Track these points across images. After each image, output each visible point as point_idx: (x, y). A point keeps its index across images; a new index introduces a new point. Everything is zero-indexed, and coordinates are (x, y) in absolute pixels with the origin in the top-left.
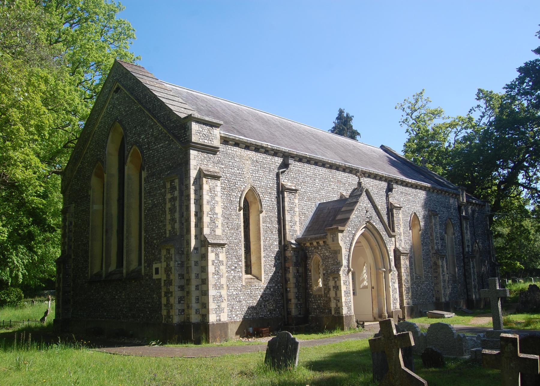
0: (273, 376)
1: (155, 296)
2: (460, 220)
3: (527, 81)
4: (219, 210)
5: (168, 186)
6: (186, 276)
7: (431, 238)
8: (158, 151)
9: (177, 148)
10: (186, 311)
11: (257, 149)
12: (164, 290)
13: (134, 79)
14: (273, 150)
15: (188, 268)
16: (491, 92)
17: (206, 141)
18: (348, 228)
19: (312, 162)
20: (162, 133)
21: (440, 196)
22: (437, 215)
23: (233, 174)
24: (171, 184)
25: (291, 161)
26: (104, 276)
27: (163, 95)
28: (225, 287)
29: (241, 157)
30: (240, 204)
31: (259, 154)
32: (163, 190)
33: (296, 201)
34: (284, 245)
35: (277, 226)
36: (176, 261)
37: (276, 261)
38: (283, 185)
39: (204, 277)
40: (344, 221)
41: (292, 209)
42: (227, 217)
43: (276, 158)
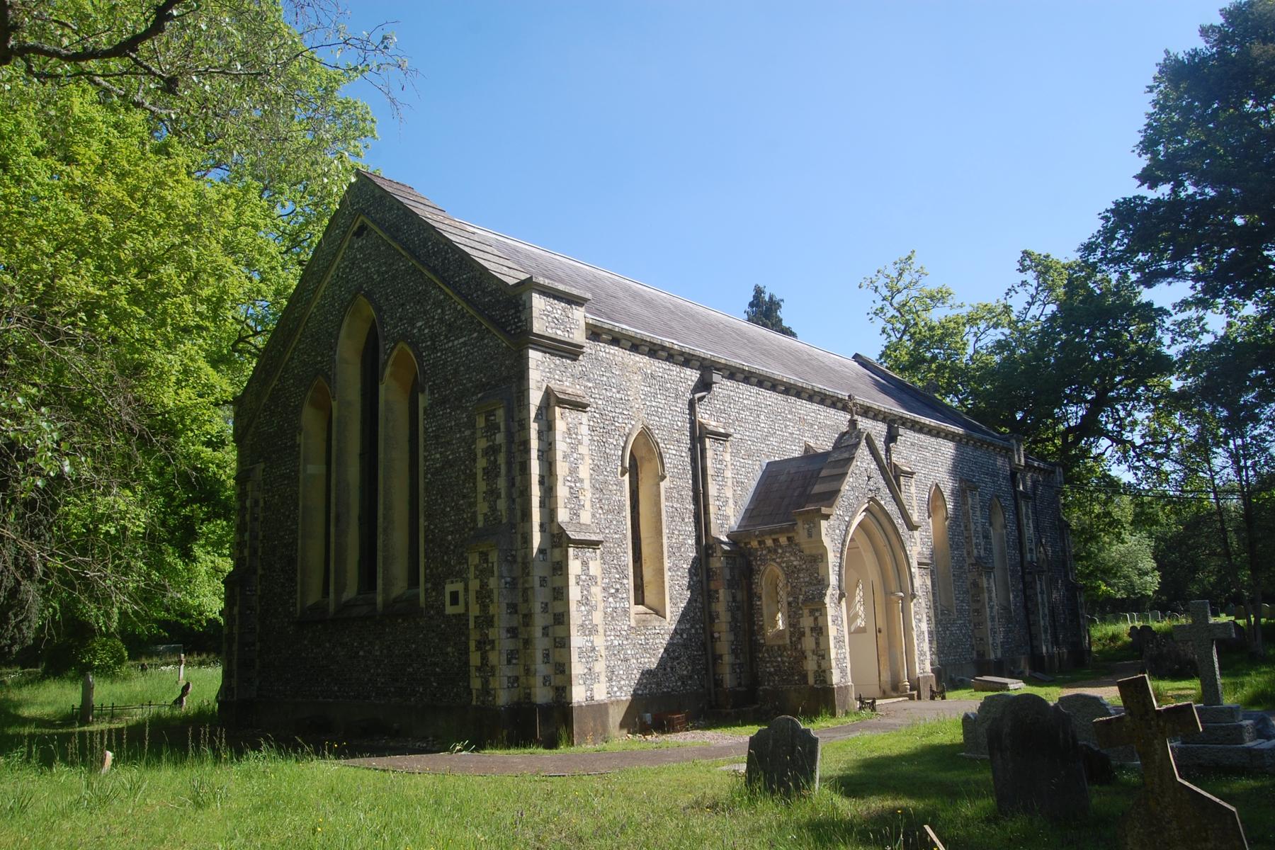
0: (769, 811)
1: (449, 649)
2: (1015, 499)
3: (1118, 236)
4: (584, 472)
5: (481, 422)
6: (522, 609)
7: (966, 534)
8: (454, 353)
9: (498, 346)
10: (523, 680)
11: (655, 351)
12: (474, 636)
13: (398, 209)
14: (682, 354)
15: (525, 591)
16: (1047, 257)
17: (559, 332)
18: (838, 511)
19: (754, 380)
20: (463, 316)
21: (978, 453)
22: (976, 488)
23: (608, 400)
24: (487, 420)
25: (716, 377)
26: (332, 608)
27: (463, 240)
28: (601, 630)
29: (624, 367)
30: (622, 461)
31: (656, 362)
32: (467, 433)
33: (728, 457)
34: (706, 546)
35: (692, 507)
36: (501, 577)
37: (691, 578)
38: (701, 424)
39: (559, 610)
40: (830, 497)
41: (719, 473)
42: (599, 489)
43: (688, 371)
